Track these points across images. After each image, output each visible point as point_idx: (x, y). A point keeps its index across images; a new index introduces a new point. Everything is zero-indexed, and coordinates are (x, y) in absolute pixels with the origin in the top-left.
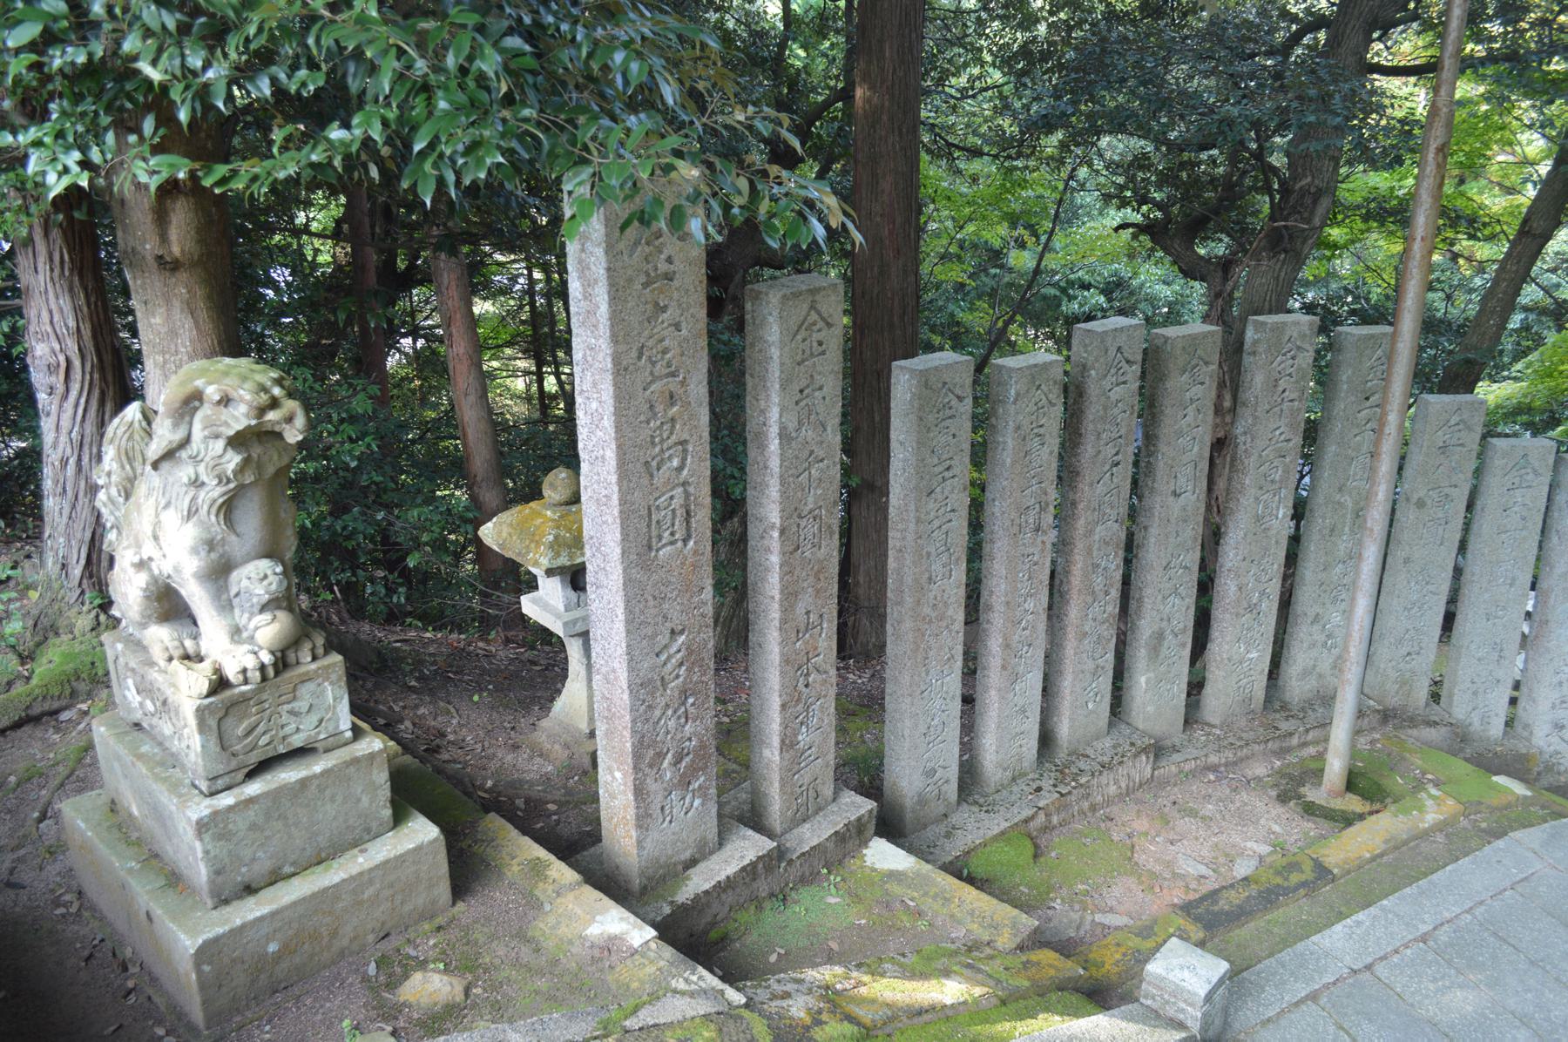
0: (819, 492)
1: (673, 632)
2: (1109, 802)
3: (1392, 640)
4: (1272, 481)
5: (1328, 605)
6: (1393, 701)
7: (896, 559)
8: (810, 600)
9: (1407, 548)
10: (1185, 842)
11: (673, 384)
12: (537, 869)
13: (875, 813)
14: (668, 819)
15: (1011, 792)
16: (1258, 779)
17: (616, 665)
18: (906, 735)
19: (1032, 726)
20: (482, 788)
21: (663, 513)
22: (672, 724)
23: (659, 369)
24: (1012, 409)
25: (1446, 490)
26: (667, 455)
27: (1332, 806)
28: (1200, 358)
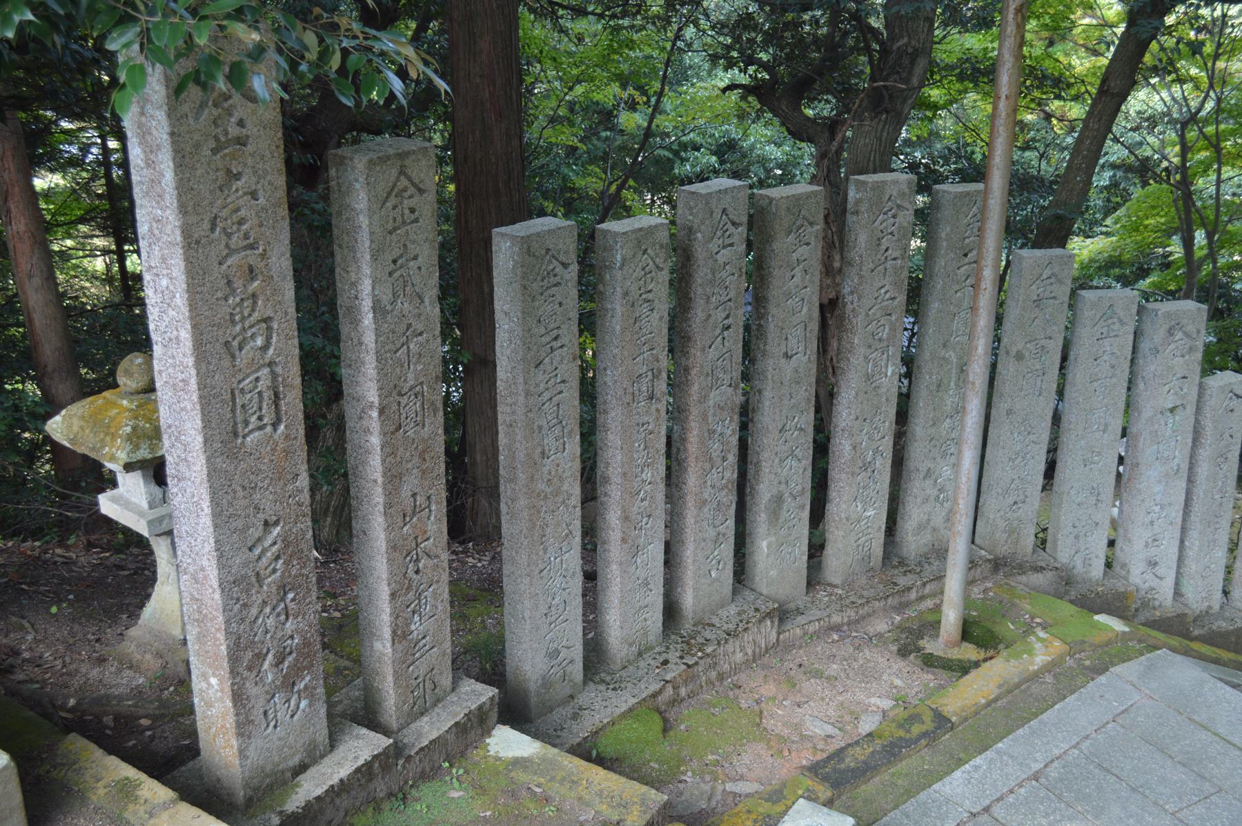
0: (420, 367)
1: (266, 523)
2: (736, 669)
4: (880, 340)
5: (938, 460)
6: (1003, 550)
7: (507, 434)
10: (811, 703)
11: (252, 258)
12: (126, 790)
13: (497, 699)
14: (272, 724)
15: (638, 668)
16: (880, 636)
17: (205, 563)
20: (63, 707)
21: (248, 396)
22: (271, 622)
23: (235, 241)
24: (619, 275)
25: (1043, 342)
28: (804, 218)
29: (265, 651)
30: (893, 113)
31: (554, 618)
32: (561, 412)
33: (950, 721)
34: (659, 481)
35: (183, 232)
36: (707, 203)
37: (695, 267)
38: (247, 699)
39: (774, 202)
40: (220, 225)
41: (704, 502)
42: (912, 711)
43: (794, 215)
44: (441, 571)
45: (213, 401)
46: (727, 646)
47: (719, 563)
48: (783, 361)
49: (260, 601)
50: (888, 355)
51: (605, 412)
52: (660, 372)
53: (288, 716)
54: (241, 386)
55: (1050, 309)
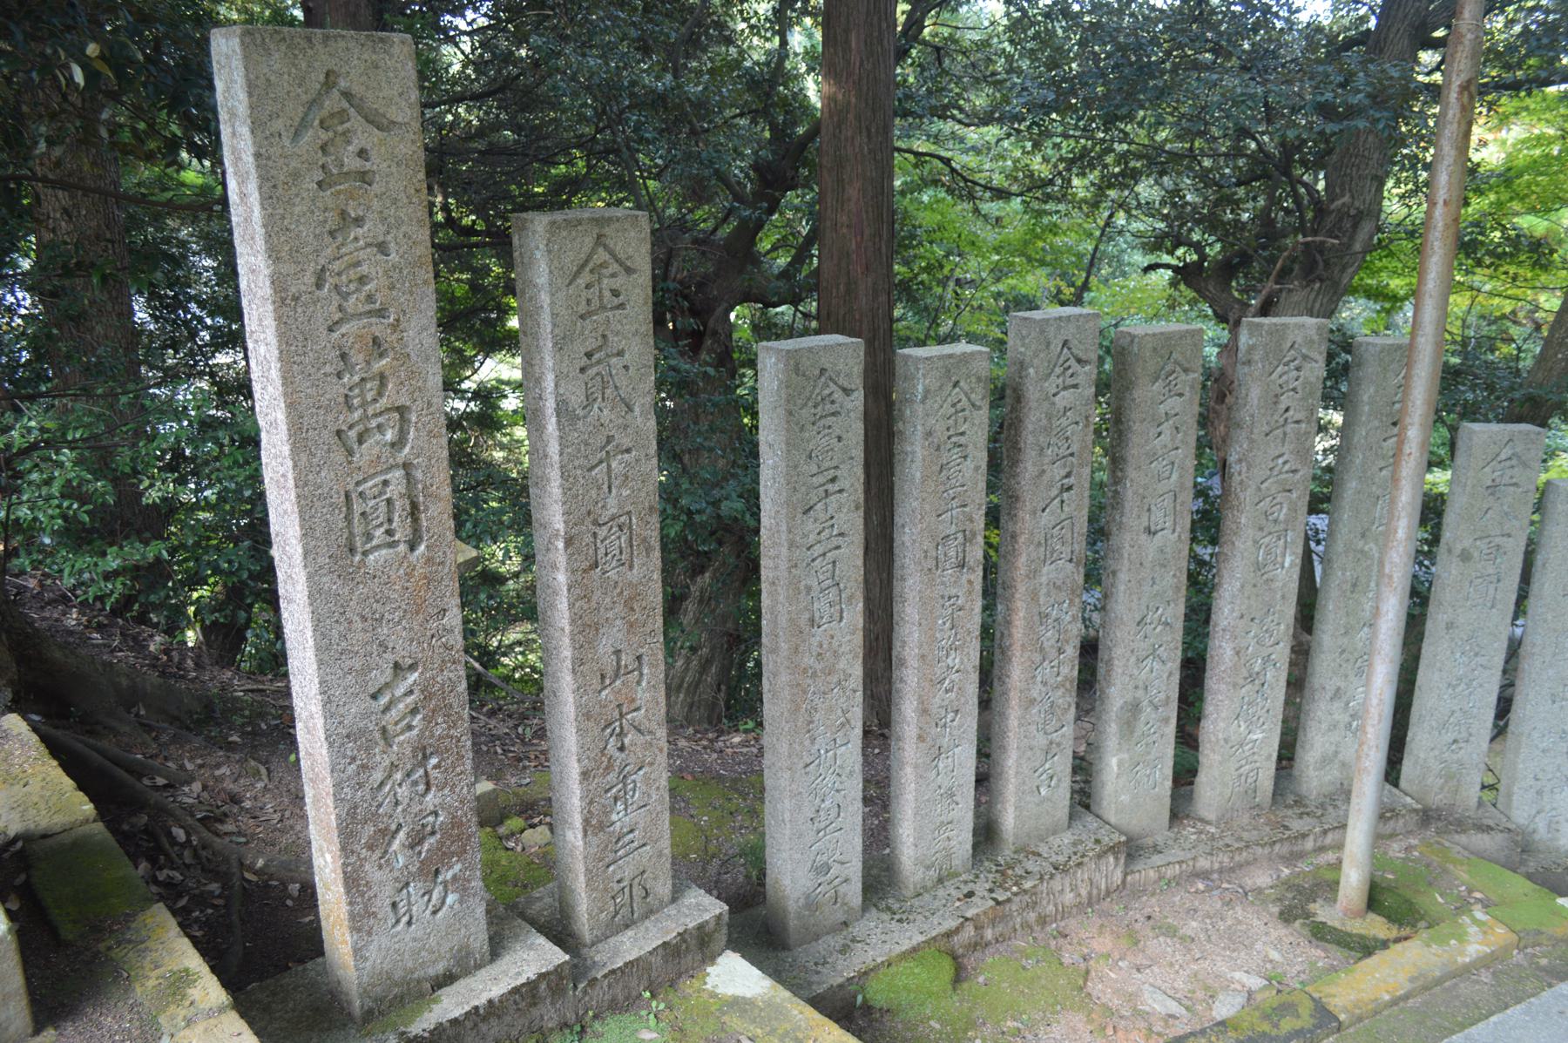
0: (625, 493)
1: (397, 666)
2: (1064, 913)
3: (1434, 723)
4: (1275, 521)
5: (1352, 678)
6: (1436, 799)
7: (770, 593)
8: (620, 635)
9: (1450, 610)
10: (1155, 969)
11: (379, 328)
12: (180, 982)
13: (726, 918)
14: (405, 919)
15: (935, 897)
16: (1259, 891)
17: (314, 709)
18: (787, 820)
19: (964, 814)
20: (251, 869)
21: (372, 503)
22: (403, 792)
23: (351, 304)
24: (919, 409)
25: (1498, 540)
26: (374, 423)
27: (1349, 929)
28: (1176, 362)
29: (393, 827)
30: (1328, 282)
31: (823, 825)
32: (837, 572)
33: (1336, 1019)
34: (970, 669)
35: (273, 283)
36: (1042, 332)
37: (1026, 410)
38: (366, 885)
39: (1136, 340)
40: (330, 281)
41: (1032, 702)
42: (1284, 998)
43: (1162, 357)
44: (657, 751)
45: (318, 504)
46: (1052, 882)
47: (1051, 778)
48: (1144, 537)
49: (387, 762)
50: (1286, 541)
51: (903, 579)
52: (974, 535)
53: (428, 912)
54: (360, 489)
55: (1510, 499)
